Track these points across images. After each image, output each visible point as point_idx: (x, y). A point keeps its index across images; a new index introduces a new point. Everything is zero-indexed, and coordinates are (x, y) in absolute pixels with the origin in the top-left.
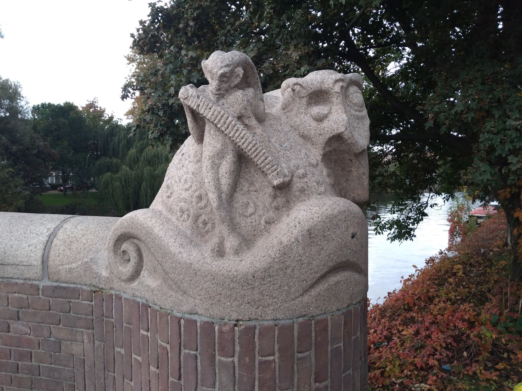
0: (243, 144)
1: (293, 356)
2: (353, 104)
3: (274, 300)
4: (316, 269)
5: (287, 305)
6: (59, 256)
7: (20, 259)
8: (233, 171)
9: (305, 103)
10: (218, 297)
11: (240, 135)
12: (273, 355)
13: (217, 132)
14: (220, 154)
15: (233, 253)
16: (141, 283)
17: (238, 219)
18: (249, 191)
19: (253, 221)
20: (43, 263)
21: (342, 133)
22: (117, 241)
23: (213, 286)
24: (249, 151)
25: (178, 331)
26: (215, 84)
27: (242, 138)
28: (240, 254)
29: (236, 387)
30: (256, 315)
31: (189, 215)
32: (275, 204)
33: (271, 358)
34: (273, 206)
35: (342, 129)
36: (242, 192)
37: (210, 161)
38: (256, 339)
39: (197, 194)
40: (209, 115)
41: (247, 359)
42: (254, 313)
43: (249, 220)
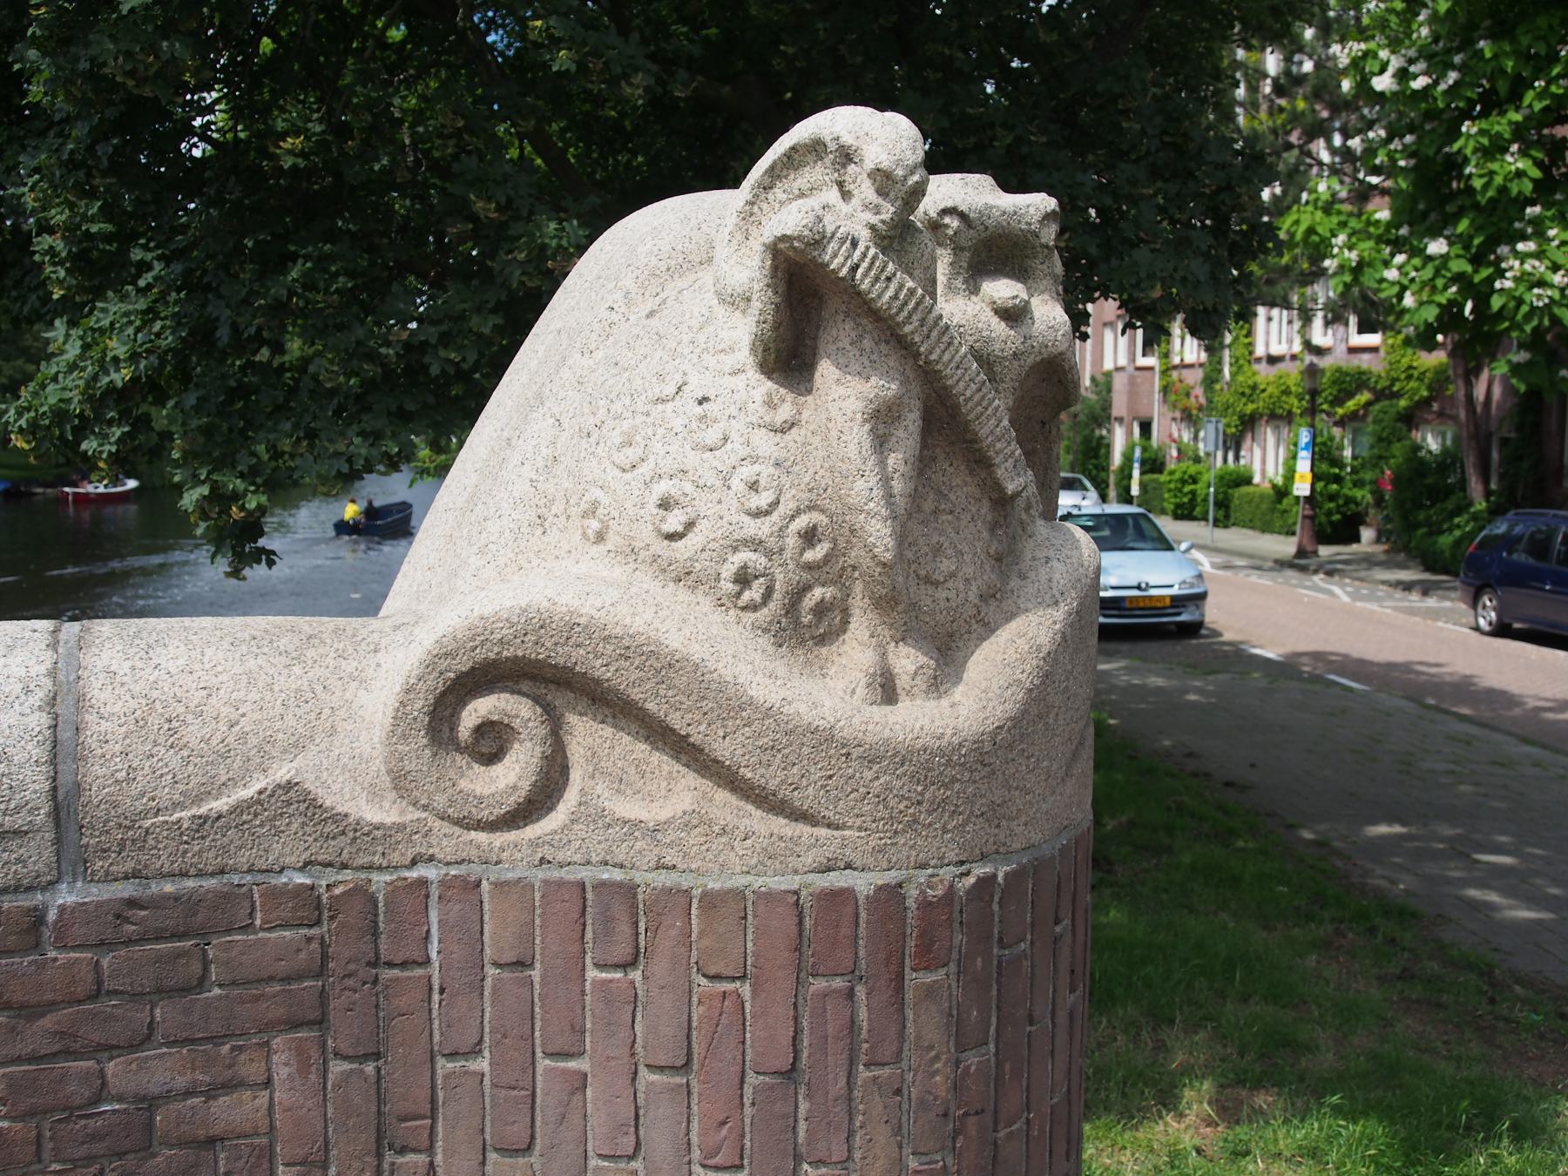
6: (130, 780)
9: (965, 265)
10: (911, 811)
13: (883, 347)
15: (924, 687)
19: (952, 595)
20: (56, 814)
21: (1061, 354)
22: (443, 694)
23: (899, 783)
25: (794, 930)
26: (892, 209)
31: (767, 595)
34: (992, 551)
37: (868, 427)
38: (996, 907)
39: (802, 522)
43: (942, 594)
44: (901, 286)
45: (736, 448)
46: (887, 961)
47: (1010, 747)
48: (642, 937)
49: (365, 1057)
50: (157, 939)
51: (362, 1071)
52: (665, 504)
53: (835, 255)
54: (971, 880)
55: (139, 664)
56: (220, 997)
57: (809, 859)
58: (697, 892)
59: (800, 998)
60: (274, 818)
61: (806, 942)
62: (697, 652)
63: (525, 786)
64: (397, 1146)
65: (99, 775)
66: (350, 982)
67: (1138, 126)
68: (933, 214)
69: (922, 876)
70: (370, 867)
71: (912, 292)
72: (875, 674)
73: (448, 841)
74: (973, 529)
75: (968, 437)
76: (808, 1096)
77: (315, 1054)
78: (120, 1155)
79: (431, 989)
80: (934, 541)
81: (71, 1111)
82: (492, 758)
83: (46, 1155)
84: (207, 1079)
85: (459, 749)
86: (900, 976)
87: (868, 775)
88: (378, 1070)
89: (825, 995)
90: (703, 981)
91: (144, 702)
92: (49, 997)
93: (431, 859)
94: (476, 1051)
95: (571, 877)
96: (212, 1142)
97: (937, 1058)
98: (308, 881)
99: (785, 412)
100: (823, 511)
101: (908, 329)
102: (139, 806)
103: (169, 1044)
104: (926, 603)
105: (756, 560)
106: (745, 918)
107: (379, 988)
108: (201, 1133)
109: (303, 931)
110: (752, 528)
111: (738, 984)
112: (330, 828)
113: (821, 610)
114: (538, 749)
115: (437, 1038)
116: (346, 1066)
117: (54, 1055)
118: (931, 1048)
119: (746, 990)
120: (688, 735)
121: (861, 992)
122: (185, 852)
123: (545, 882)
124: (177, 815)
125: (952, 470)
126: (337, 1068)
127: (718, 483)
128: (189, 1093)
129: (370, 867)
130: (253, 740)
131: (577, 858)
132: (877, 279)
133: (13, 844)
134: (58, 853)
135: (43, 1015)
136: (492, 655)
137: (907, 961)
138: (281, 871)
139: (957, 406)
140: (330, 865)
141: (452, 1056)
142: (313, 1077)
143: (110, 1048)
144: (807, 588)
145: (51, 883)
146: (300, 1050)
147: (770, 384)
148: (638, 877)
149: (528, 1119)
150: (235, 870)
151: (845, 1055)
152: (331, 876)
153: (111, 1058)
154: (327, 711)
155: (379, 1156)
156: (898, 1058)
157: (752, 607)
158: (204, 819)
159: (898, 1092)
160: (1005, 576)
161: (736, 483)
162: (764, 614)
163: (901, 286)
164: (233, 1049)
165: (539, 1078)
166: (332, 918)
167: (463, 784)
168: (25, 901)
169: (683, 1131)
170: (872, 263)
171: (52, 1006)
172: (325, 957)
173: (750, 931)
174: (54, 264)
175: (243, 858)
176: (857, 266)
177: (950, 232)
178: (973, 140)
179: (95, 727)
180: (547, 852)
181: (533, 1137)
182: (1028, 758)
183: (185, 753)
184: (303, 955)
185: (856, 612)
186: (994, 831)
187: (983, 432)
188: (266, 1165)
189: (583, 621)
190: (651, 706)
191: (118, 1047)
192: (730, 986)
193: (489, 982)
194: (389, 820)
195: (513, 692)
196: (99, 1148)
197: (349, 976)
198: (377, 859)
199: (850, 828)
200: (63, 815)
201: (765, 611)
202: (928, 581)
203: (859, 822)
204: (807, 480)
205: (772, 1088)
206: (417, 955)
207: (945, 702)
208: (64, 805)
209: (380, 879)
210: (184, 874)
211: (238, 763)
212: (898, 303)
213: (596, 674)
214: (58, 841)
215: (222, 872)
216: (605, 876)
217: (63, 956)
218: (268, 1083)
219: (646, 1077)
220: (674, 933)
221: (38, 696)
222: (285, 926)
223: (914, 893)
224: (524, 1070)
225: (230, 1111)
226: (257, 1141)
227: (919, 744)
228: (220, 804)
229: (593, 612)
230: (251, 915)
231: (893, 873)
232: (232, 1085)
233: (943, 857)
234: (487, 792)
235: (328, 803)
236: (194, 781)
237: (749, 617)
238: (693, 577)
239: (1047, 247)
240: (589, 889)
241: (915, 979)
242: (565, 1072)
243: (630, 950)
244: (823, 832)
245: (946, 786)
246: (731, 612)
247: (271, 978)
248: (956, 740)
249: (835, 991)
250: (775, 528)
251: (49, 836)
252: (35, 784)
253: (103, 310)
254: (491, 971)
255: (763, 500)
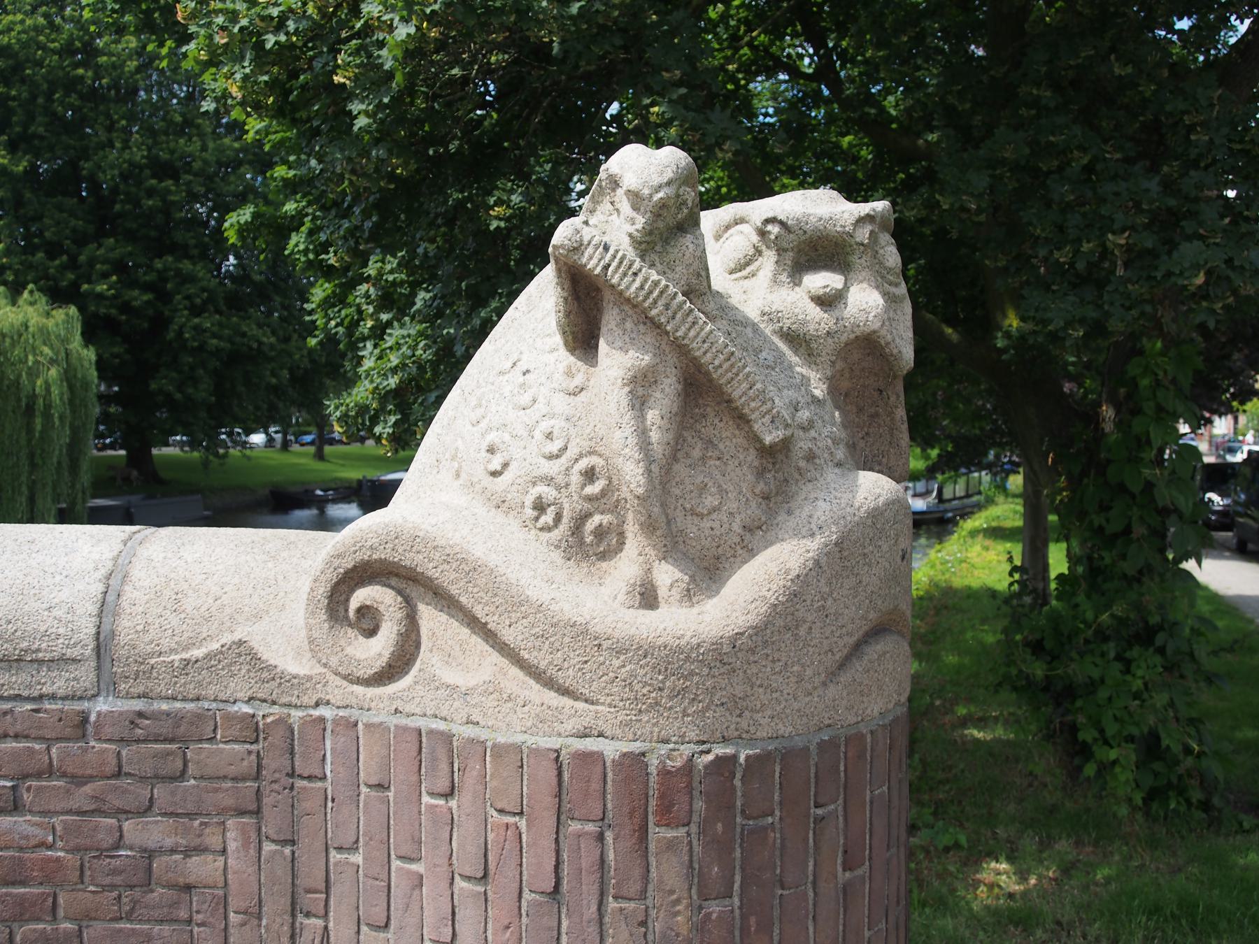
0: (705, 353)
1: (808, 815)
2: (885, 268)
3: (774, 695)
4: (850, 626)
5: (796, 705)
6: (145, 631)
7: (25, 645)
8: (676, 414)
9: (789, 263)
10: (653, 695)
11: (698, 334)
12: (772, 814)
13: (641, 327)
14: (650, 375)
16: (433, 682)
17: (680, 520)
18: (703, 459)
19: (716, 525)
20: (98, 649)
21: (875, 332)
22: (337, 584)
23: (642, 672)
24: (716, 368)
25: (554, 781)
27: (704, 342)
28: (695, 600)
29: (694, 891)
30: (737, 730)
31: (558, 518)
32: (760, 487)
33: (770, 820)
34: (757, 491)
35: (877, 325)
36: (688, 462)
37: (627, 389)
38: (737, 782)
39: (583, 464)
40: (633, 289)
41: (719, 826)
42: (733, 727)
43: (706, 524)
44: (646, 280)
45: (541, 407)
46: (631, 815)
47: (752, 651)
48: (456, 774)
49: (284, 843)
50: (156, 741)
51: (282, 852)
52: (491, 450)
53: (591, 258)
54: (710, 757)
55: (169, 555)
56: (193, 787)
57: (569, 726)
58: (489, 744)
59: (561, 835)
60: (231, 665)
61: (565, 792)
62: (493, 560)
63: (387, 655)
64: (305, 911)
65: (126, 627)
66: (275, 786)
67: (1207, 138)
68: (759, 224)
69: (664, 749)
70: (289, 705)
71: (656, 283)
72: (635, 584)
73: (339, 691)
74: (740, 474)
75: (726, 398)
76: (569, 916)
77: (254, 836)
78: (132, 887)
79: (326, 798)
80: (698, 481)
81: (102, 852)
82: (371, 632)
83: (87, 879)
84: (184, 842)
85: (350, 625)
86: (644, 829)
87: (617, 663)
88: (293, 853)
89: (579, 836)
90: (495, 814)
91: (163, 580)
92: (89, 772)
93: (328, 703)
94: (354, 848)
95: (412, 725)
96: (188, 888)
97: (678, 901)
98: (251, 711)
99: (578, 380)
100: (600, 456)
101: (654, 312)
102: (149, 649)
103: (165, 814)
104: (692, 531)
105: (548, 493)
106: (522, 767)
107: (295, 793)
108: (181, 881)
109: (247, 746)
110: (553, 468)
111: (517, 818)
112: (265, 675)
113: (600, 533)
114: (396, 628)
115: (330, 835)
116: (273, 847)
117: (93, 811)
118: (672, 892)
119: (523, 824)
120: (486, 623)
121: (609, 836)
122: (176, 683)
123: (396, 726)
124: (172, 657)
125: (722, 425)
126: (268, 847)
127: (525, 434)
128: (173, 851)
129: (289, 705)
130: (228, 611)
131: (418, 711)
132: (625, 275)
133: (72, 668)
134: (98, 676)
135: (86, 784)
136: (366, 558)
137: (651, 817)
138: (235, 702)
139: (708, 373)
140: (264, 701)
141: (340, 849)
142: (252, 851)
143: (126, 812)
144: (589, 515)
145: (94, 696)
146: (243, 831)
147: (572, 359)
148: (457, 729)
149: (385, 904)
150: (206, 699)
151: (596, 886)
152: (266, 709)
153: (127, 819)
154: (282, 594)
155: (293, 916)
156: (643, 895)
157: (547, 529)
158: (188, 661)
159: (643, 923)
160: (772, 513)
161: (538, 434)
162: (556, 534)
163: (646, 280)
164: (202, 823)
165: (393, 874)
166: (265, 739)
167: (349, 650)
168: (78, 706)
169: (482, 930)
170: (621, 263)
171: (91, 778)
172: (259, 766)
173: (525, 777)
174: (368, 304)
175: (211, 691)
176: (609, 265)
177: (772, 237)
178: (1056, 163)
179: (129, 593)
180: (398, 704)
181: (388, 918)
182: (773, 661)
183: (183, 616)
184: (245, 763)
185: (629, 535)
186: (735, 719)
187: (736, 395)
188: (222, 911)
189: (421, 534)
190: (463, 600)
191: (129, 812)
192: (511, 820)
193: (362, 797)
194: (302, 671)
195: (385, 585)
196: (118, 880)
197: (275, 782)
198: (294, 700)
199: (603, 704)
200: (102, 651)
201: (556, 531)
202: (694, 513)
203: (609, 699)
204: (588, 431)
205: (540, 904)
206: (318, 772)
207: (696, 610)
208: (102, 645)
209: (296, 714)
210: (175, 699)
211: (216, 625)
212: (643, 293)
213: (430, 574)
214: (98, 668)
215: (198, 699)
216: (434, 726)
217: (98, 746)
218: (224, 851)
219: (460, 883)
220: (475, 773)
221: (103, 571)
222: (235, 741)
223: (656, 762)
224: (383, 866)
225: (202, 868)
226: (216, 892)
227: (660, 641)
228: (198, 653)
229: (429, 528)
230: (215, 730)
231: (638, 744)
232: (201, 850)
233: (683, 736)
234: (363, 657)
235: (264, 658)
236: (186, 635)
237: (545, 536)
238: (506, 504)
239: (862, 244)
240: (424, 734)
241: (658, 834)
242: (409, 872)
243: (447, 784)
244: (580, 705)
245: (686, 678)
246: (533, 532)
247: (225, 777)
248: (694, 641)
249: (586, 833)
250: (563, 468)
251: (93, 664)
252: (87, 629)
253: (390, 335)
254: (364, 789)
255: (554, 447)
